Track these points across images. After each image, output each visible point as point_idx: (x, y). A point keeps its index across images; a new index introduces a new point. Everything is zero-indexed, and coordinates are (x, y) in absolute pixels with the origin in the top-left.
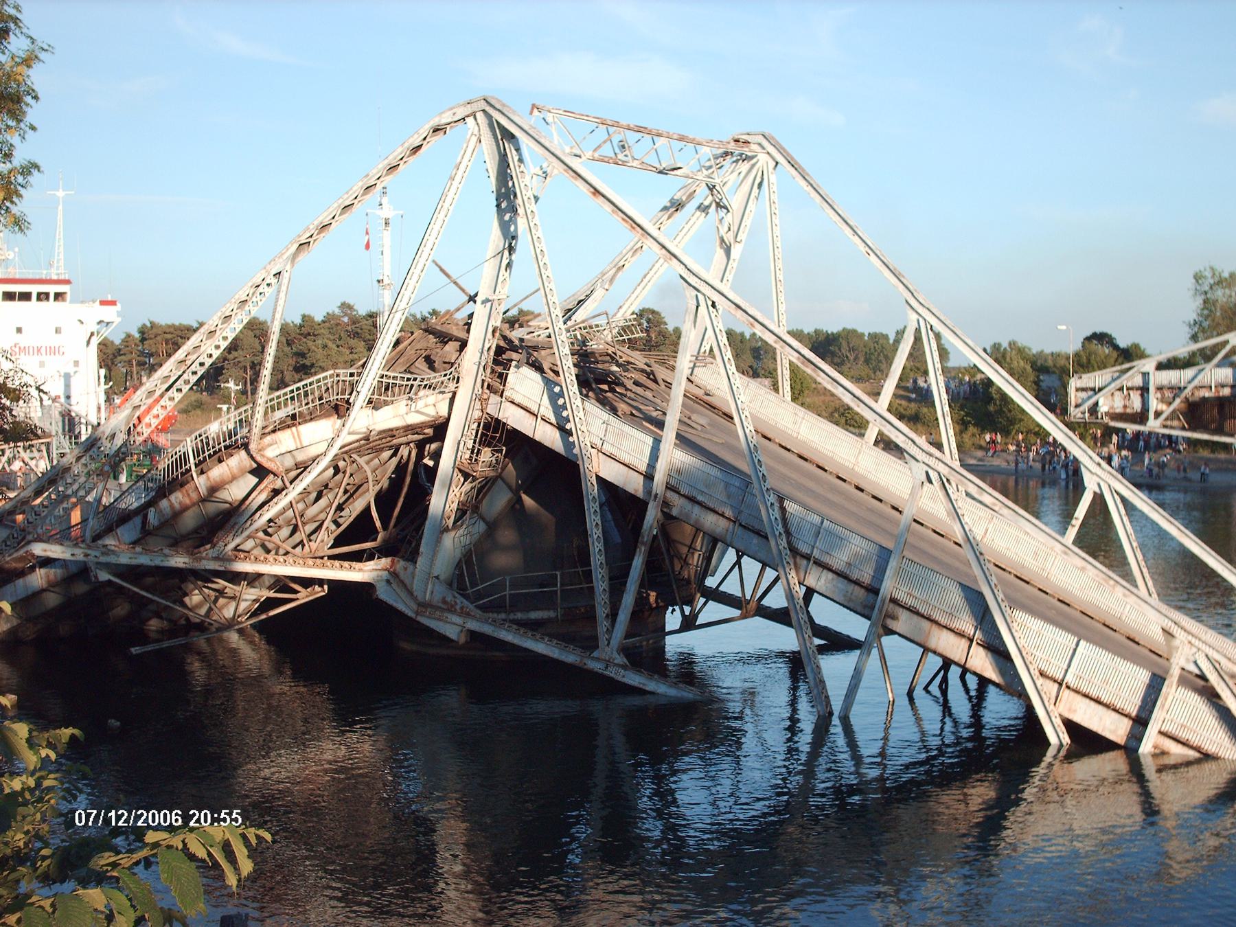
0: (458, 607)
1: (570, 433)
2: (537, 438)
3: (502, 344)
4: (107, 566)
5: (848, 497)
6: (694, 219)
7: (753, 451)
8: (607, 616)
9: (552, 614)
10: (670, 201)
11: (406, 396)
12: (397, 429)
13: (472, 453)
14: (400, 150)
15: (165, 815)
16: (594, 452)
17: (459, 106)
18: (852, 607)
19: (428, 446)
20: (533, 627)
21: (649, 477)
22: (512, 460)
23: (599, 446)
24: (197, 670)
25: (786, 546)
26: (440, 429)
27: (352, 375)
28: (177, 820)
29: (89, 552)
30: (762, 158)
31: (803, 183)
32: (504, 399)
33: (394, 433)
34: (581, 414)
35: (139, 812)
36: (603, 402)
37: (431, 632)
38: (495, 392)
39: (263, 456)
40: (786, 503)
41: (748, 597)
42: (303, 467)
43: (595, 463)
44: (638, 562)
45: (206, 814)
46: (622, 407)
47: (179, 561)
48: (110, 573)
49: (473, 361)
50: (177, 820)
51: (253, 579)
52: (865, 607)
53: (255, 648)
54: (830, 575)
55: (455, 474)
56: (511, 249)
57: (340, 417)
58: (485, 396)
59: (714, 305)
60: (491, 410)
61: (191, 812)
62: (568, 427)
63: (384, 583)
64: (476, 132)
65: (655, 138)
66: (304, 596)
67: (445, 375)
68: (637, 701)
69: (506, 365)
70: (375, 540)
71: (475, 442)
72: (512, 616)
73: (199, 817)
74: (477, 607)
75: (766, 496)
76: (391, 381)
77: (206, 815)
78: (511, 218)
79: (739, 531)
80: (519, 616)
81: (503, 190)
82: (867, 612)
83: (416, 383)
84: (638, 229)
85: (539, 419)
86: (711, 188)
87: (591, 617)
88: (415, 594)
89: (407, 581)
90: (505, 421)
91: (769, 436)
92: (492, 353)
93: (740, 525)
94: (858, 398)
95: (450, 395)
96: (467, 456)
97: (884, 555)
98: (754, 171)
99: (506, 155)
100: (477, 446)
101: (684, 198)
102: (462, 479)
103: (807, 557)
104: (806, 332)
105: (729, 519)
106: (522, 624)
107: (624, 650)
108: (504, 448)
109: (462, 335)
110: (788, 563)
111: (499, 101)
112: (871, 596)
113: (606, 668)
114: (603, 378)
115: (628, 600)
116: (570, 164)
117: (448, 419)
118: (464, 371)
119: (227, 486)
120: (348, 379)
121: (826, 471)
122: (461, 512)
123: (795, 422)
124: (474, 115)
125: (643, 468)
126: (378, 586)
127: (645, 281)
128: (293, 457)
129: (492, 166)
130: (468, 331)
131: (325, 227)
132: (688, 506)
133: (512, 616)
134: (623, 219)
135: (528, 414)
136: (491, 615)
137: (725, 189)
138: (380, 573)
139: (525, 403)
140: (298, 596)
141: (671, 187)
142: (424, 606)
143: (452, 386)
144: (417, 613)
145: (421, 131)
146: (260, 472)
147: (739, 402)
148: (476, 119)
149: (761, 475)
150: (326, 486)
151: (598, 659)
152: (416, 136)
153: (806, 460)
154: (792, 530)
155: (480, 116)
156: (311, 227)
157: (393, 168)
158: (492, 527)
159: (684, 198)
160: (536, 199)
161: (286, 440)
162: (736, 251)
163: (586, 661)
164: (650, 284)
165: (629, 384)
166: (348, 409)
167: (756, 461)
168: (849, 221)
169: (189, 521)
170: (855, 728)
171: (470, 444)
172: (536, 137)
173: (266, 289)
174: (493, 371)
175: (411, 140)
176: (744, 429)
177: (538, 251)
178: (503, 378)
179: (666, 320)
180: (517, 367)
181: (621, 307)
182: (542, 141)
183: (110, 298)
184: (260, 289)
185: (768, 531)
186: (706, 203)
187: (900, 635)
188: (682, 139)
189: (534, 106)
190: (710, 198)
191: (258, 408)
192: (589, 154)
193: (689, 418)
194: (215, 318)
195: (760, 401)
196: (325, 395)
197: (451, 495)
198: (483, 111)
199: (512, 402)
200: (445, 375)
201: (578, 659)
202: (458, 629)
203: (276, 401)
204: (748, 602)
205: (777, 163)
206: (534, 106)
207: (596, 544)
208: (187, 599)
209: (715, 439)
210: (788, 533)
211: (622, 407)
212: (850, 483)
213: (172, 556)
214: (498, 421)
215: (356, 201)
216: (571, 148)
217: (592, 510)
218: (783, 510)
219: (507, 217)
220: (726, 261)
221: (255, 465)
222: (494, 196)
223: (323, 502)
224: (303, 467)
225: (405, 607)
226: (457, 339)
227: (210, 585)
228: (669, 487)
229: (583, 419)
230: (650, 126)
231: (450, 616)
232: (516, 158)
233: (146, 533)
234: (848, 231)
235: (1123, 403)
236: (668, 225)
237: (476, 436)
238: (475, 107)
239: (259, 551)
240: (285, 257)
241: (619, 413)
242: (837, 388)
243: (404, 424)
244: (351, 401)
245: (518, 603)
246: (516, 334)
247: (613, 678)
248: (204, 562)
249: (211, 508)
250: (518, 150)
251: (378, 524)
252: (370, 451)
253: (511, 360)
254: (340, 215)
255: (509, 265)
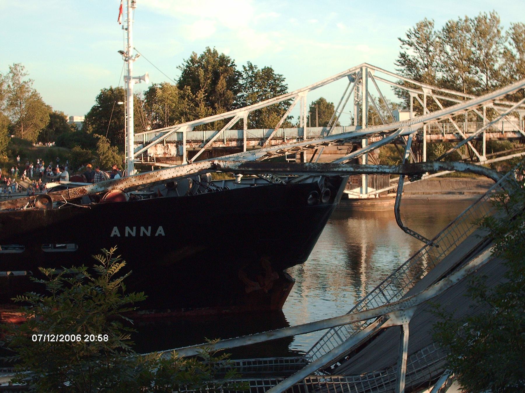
73: (64, 338)
235: (163, 151)
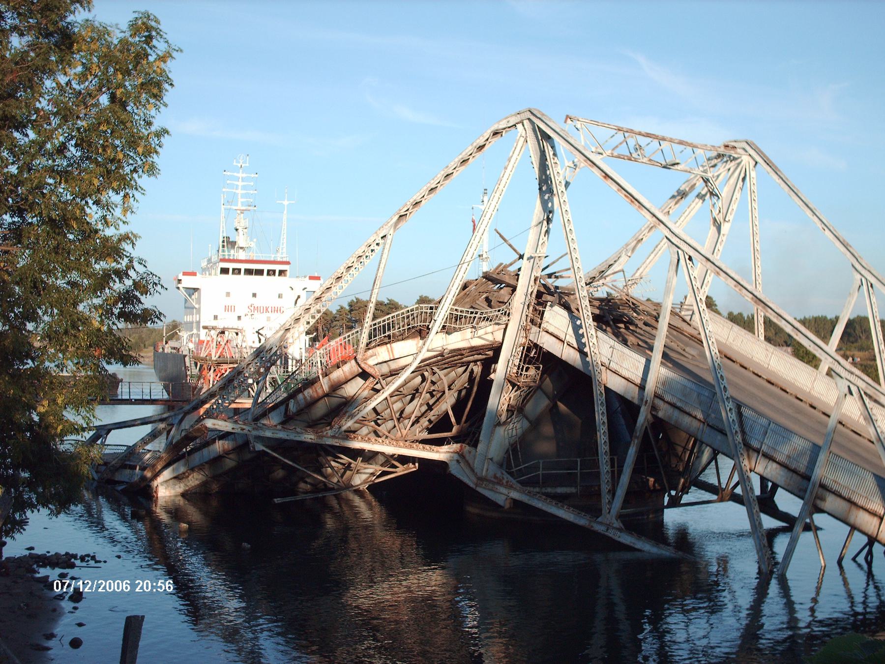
0: (504, 481)
1: (586, 355)
2: (564, 358)
3: (542, 289)
4: (259, 438)
5: (763, 389)
6: (694, 204)
7: (715, 369)
8: (609, 491)
9: (573, 490)
10: (677, 192)
11: (470, 325)
12: (464, 349)
13: (518, 369)
14: (470, 148)
15: (118, 584)
16: (603, 368)
17: (512, 116)
18: (790, 489)
19: (493, 365)
20: (560, 499)
21: (642, 387)
22: (549, 375)
23: (607, 364)
24: (330, 523)
25: (741, 441)
26: (497, 349)
27: (431, 308)
28: (127, 588)
29: (244, 427)
30: (745, 159)
31: (775, 177)
32: (541, 330)
33: (464, 352)
34: (594, 340)
35: (100, 582)
36: (617, 335)
37: (486, 500)
38: (535, 325)
39: (366, 363)
40: (743, 409)
41: (724, 486)
42: (394, 373)
43: (604, 376)
44: (632, 452)
45: (147, 583)
46: (631, 339)
47: (309, 437)
48: (264, 446)
49: (520, 301)
50: (127, 588)
51: (370, 457)
52: (800, 490)
53: (371, 508)
54: (775, 465)
55: (506, 384)
56: (549, 220)
57: (422, 338)
58: (528, 328)
59: (690, 258)
60: (531, 337)
61: (137, 582)
62: (585, 350)
63: (455, 462)
64: (524, 134)
65: (661, 142)
66: (401, 470)
67: (499, 311)
68: (628, 556)
69: (544, 304)
70: (451, 430)
71: (520, 361)
72: (544, 490)
74: (519, 482)
75: (726, 403)
76: (459, 314)
77: (147, 584)
78: (549, 197)
79: (707, 430)
80: (549, 490)
81: (544, 177)
82: (801, 494)
83: (478, 316)
84: (636, 202)
85: (566, 344)
86: (706, 181)
87: (598, 494)
88: (476, 471)
89: (471, 462)
90: (541, 345)
91: (745, 366)
92: (534, 296)
93: (708, 425)
94: (797, 329)
95: (504, 326)
96: (515, 371)
97: (816, 449)
98: (740, 167)
99: (544, 151)
100: (522, 364)
101: (687, 189)
102: (511, 388)
103: (757, 451)
104: (829, 317)
105: (699, 420)
106: (548, 495)
107: (620, 517)
108: (541, 366)
109: (512, 282)
110: (741, 454)
111: (539, 111)
112: (805, 482)
113: (607, 530)
114: (618, 319)
115: (625, 479)
116: (588, 156)
117: (502, 344)
118: (514, 309)
119: (343, 386)
120: (429, 311)
121: (787, 393)
122: (510, 410)
123: (767, 356)
124: (522, 122)
125: (638, 381)
126: (450, 464)
127: (657, 250)
128: (389, 366)
129: (535, 160)
130: (517, 280)
131: (417, 204)
132: (670, 410)
133: (544, 490)
134: (625, 196)
135: (558, 341)
136: (528, 488)
137: (717, 183)
138: (452, 455)
139: (556, 332)
140: (397, 470)
141: (676, 180)
142: (481, 479)
143: (505, 318)
144: (477, 485)
145: (485, 134)
146: (364, 375)
147: (707, 332)
148: (523, 125)
149: (722, 387)
150: (417, 390)
151: (601, 523)
152: (481, 138)
153: (773, 384)
154: (747, 430)
155: (526, 122)
156: (408, 203)
157: (464, 162)
158: (535, 424)
159: (687, 189)
160: (567, 184)
161: (382, 353)
162: (725, 228)
163: (592, 524)
164: (660, 252)
165: (640, 324)
166: (428, 333)
167: (719, 376)
168: (810, 205)
169: (320, 409)
170: (790, 584)
171: (517, 362)
172: (565, 137)
173: (376, 247)
174: (535, 310)
175: (478, 141)
176: (711, 350)
177: (566, 221)
178: (542, 314)
179: (716, 303)
180: (551, 306)
181: (638, 269)
182: (569, 140)
183: (316, 275)
184: (372, 247)
185: (727, 429)
186: (703, 192)
187: (829, 514)
188: (681, 143)
189: (567, 117)
190: (706, 189)
191: (364, 330)
192: (609, 152)
193: (684, 350)
194: (342, 268)
195: (741, 341)
196: (411, 322)
197: (502, 399)
198: (529, 119)
199: (547, 332)
200: (499, 311)
201: (587, 523)
202: (504, 497)
203: (377, 325)
204: (723, 490)
205: (756, 163)
206: (567, 117)
207: (603, 437)
208: (324, 470)
209: (701, 365)
210: (743, 433)
211: (631, 339)
212: (806, 403)
213: (302, 433)
214: (536, 346)
215: (439, 185)
216: (596, 148)
217: (600, 412)
218: (740, 415)
219: (546, 197)
220: (717, 235)
221: (361, 371)
222: (537, 182)
223: (415, 402)
224: (394, 373)
225: (468, 480)
226: (508, 285)
227: (339, 460)
228: (657, 396)
229: (596, 343)
230: (657, 134)
231: (498, 487)
232: (551, 153)
233: (288, 420)
234: (809, 212)
236: (675, 209)
237: (521, 357)
238: (523, 116)
239: (372, 436)
240: (389, 225)
241: (629, 343)
242: (781, 321)
243: (469, 346)
244: (430, 327)
245: (548, 480)
246: (550, 282)
247: (611, 538)
248: (325, 439)
249: (335, 401)
250: (553, 147)
251: (453, 420)
252: (446, 366)
253: (547, 302)
254: (428, 195)
255: (547, 232)
